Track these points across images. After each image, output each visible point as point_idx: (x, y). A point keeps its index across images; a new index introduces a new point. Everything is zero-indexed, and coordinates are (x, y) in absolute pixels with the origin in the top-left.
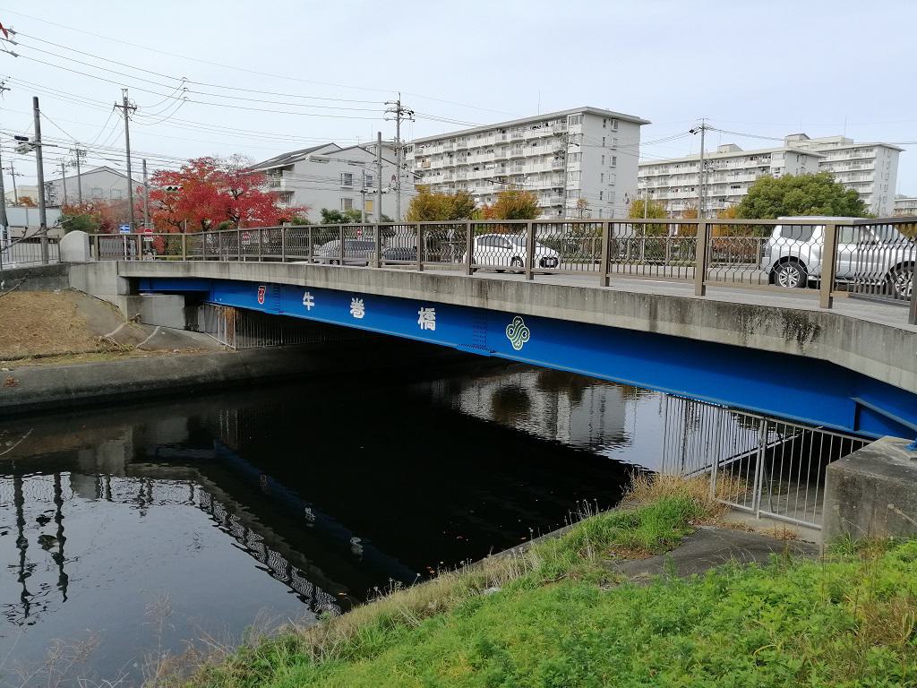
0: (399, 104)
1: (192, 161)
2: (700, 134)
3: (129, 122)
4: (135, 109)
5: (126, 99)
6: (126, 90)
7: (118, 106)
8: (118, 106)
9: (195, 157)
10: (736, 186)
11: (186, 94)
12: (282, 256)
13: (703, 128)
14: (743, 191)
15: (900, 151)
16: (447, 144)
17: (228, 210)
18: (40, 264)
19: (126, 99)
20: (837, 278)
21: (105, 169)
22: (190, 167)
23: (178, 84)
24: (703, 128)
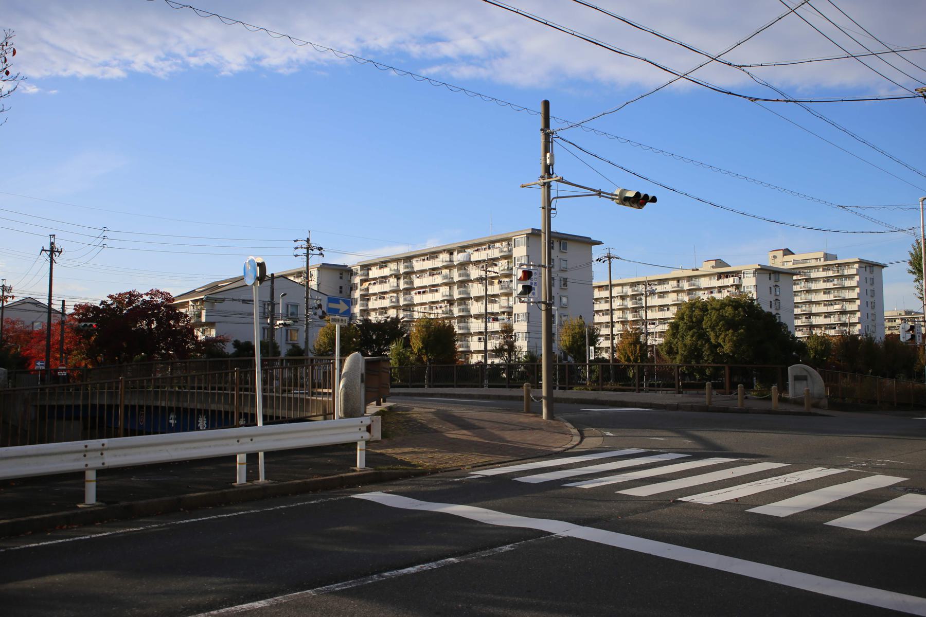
0: (308, 240)
1: (110, 297)
2: (607, 262)
3: (54, 264)
4: (60, 252)
5: (52, 244)
6: (54, 235)
7: (45, 251)
8: (45, 251)
9: (114, 293)
10: (662, 308)
11: (105, 242)
12: (408, 384)
13: (610, 258)
14: (670, 314)
15: (883, 266)
16: (393, 266)
17: (147, 341)
18: (276, 312)
19: (52, 244)
20: (330, 394)
21: (30, 298)
22: (109, 303)
23: (98, 233)
24: (610, 258)
